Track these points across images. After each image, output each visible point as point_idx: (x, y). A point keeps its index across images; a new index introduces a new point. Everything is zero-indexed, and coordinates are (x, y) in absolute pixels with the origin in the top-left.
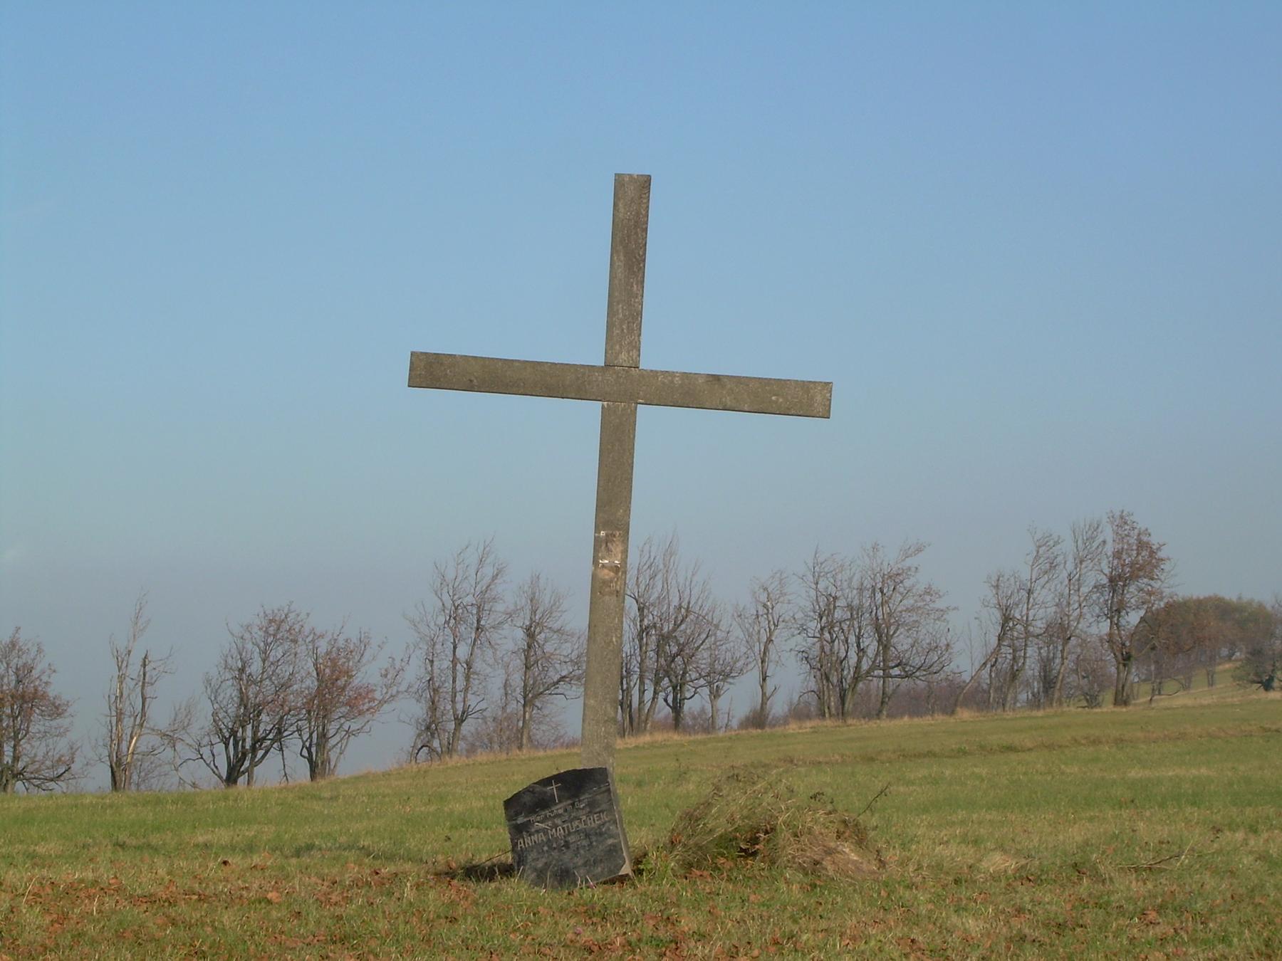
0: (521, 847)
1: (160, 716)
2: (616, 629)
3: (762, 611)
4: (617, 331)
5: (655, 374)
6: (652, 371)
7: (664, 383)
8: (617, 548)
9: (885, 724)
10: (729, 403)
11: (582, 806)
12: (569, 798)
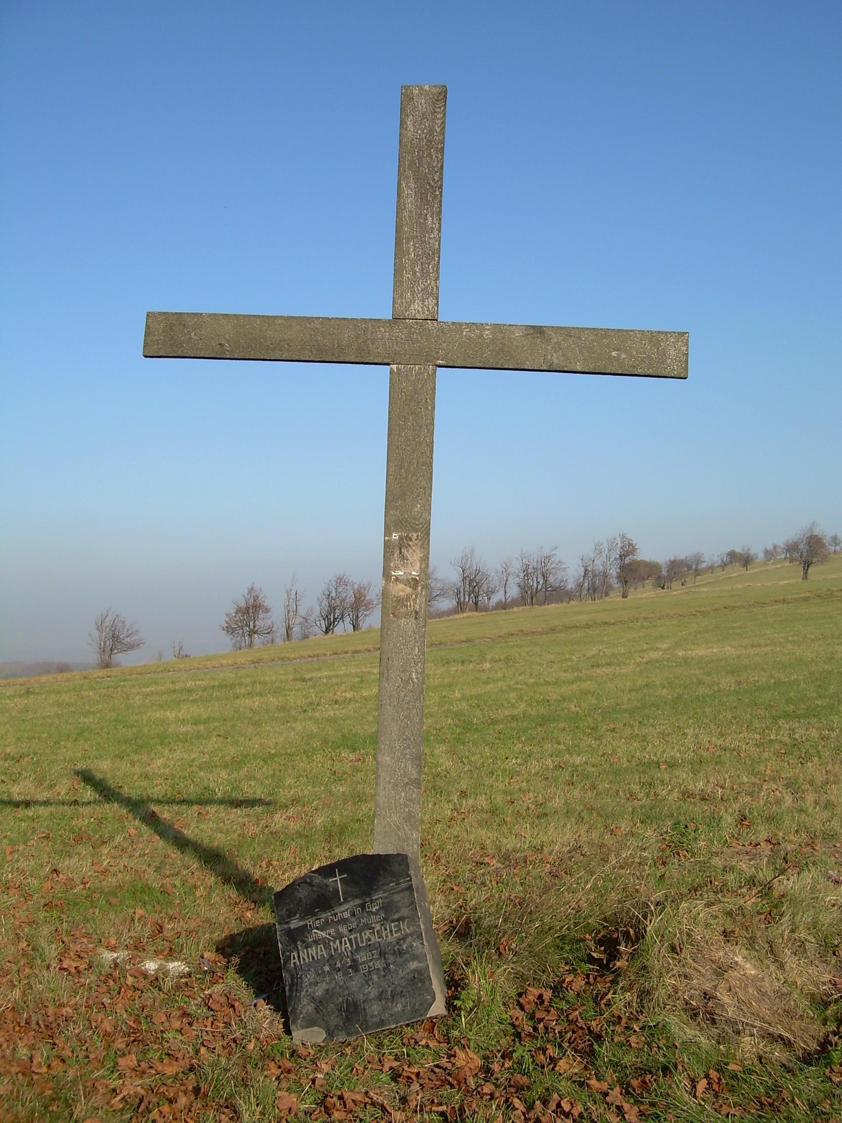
0: (295, 963)
1: (302, 611)
2: (416, 663)
3: (504, 570)
4: (407, 275)
5: (458, 327)
6: (453, 323)
7: (469, 338)
8: (414, 555)
9: (546, 607)
10: (556, 361)
11: (374, 910)
12: (356, 897)
